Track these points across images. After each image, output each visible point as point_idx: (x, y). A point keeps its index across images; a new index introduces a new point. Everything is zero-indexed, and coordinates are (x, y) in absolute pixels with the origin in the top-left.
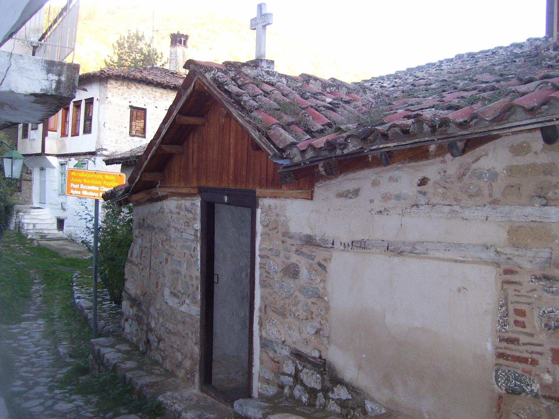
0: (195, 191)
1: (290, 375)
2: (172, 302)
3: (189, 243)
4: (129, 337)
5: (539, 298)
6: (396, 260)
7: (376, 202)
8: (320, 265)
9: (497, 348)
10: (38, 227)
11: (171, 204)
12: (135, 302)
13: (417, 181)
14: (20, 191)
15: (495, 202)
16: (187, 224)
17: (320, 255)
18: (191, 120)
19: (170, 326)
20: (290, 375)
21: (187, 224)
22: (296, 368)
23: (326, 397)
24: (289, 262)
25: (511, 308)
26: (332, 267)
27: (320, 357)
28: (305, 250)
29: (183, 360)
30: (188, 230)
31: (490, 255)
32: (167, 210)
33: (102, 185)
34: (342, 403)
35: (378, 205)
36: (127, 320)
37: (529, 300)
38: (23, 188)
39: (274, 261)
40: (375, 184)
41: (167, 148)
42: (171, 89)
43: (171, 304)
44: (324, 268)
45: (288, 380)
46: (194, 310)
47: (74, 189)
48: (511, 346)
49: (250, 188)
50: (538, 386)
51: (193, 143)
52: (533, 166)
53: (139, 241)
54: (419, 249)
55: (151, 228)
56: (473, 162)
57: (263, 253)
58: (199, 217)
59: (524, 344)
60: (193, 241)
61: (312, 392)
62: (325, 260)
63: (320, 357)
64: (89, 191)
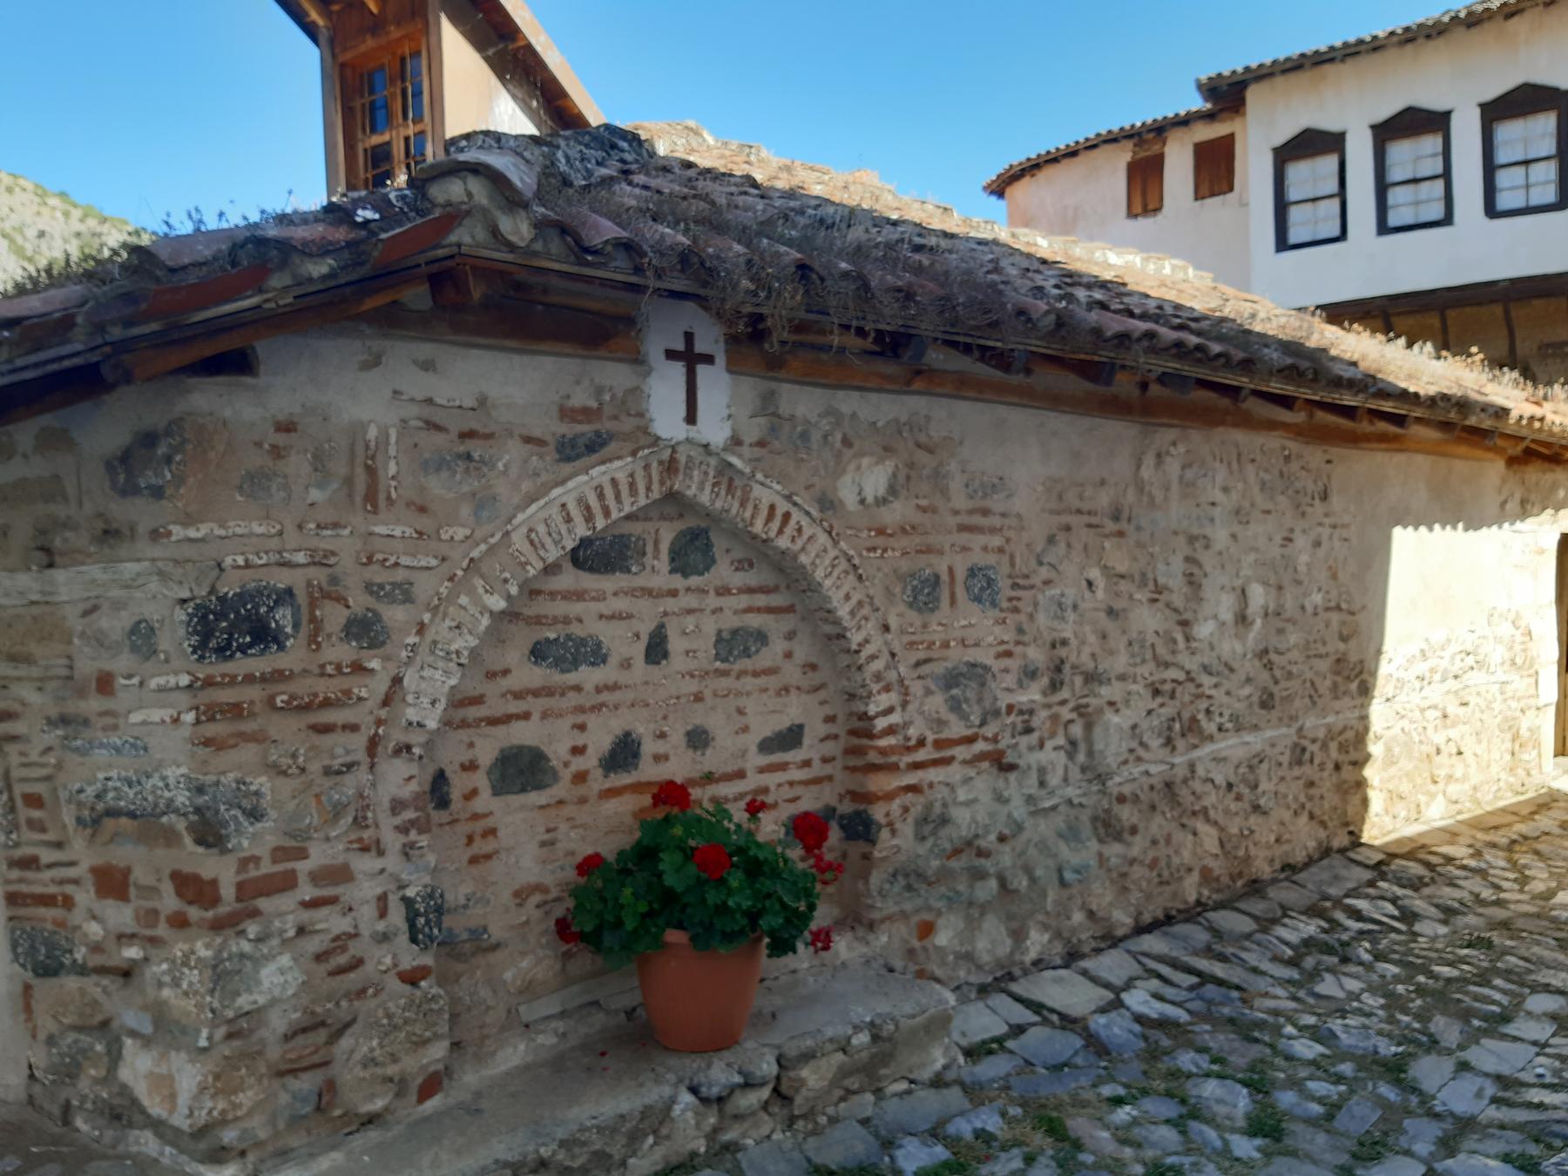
5: (59, 766)
25: (18, 790)
37: (44, 772)
42: (696, 279)
48: (30, 875)
50: (83, 949)
59: (50, 866)
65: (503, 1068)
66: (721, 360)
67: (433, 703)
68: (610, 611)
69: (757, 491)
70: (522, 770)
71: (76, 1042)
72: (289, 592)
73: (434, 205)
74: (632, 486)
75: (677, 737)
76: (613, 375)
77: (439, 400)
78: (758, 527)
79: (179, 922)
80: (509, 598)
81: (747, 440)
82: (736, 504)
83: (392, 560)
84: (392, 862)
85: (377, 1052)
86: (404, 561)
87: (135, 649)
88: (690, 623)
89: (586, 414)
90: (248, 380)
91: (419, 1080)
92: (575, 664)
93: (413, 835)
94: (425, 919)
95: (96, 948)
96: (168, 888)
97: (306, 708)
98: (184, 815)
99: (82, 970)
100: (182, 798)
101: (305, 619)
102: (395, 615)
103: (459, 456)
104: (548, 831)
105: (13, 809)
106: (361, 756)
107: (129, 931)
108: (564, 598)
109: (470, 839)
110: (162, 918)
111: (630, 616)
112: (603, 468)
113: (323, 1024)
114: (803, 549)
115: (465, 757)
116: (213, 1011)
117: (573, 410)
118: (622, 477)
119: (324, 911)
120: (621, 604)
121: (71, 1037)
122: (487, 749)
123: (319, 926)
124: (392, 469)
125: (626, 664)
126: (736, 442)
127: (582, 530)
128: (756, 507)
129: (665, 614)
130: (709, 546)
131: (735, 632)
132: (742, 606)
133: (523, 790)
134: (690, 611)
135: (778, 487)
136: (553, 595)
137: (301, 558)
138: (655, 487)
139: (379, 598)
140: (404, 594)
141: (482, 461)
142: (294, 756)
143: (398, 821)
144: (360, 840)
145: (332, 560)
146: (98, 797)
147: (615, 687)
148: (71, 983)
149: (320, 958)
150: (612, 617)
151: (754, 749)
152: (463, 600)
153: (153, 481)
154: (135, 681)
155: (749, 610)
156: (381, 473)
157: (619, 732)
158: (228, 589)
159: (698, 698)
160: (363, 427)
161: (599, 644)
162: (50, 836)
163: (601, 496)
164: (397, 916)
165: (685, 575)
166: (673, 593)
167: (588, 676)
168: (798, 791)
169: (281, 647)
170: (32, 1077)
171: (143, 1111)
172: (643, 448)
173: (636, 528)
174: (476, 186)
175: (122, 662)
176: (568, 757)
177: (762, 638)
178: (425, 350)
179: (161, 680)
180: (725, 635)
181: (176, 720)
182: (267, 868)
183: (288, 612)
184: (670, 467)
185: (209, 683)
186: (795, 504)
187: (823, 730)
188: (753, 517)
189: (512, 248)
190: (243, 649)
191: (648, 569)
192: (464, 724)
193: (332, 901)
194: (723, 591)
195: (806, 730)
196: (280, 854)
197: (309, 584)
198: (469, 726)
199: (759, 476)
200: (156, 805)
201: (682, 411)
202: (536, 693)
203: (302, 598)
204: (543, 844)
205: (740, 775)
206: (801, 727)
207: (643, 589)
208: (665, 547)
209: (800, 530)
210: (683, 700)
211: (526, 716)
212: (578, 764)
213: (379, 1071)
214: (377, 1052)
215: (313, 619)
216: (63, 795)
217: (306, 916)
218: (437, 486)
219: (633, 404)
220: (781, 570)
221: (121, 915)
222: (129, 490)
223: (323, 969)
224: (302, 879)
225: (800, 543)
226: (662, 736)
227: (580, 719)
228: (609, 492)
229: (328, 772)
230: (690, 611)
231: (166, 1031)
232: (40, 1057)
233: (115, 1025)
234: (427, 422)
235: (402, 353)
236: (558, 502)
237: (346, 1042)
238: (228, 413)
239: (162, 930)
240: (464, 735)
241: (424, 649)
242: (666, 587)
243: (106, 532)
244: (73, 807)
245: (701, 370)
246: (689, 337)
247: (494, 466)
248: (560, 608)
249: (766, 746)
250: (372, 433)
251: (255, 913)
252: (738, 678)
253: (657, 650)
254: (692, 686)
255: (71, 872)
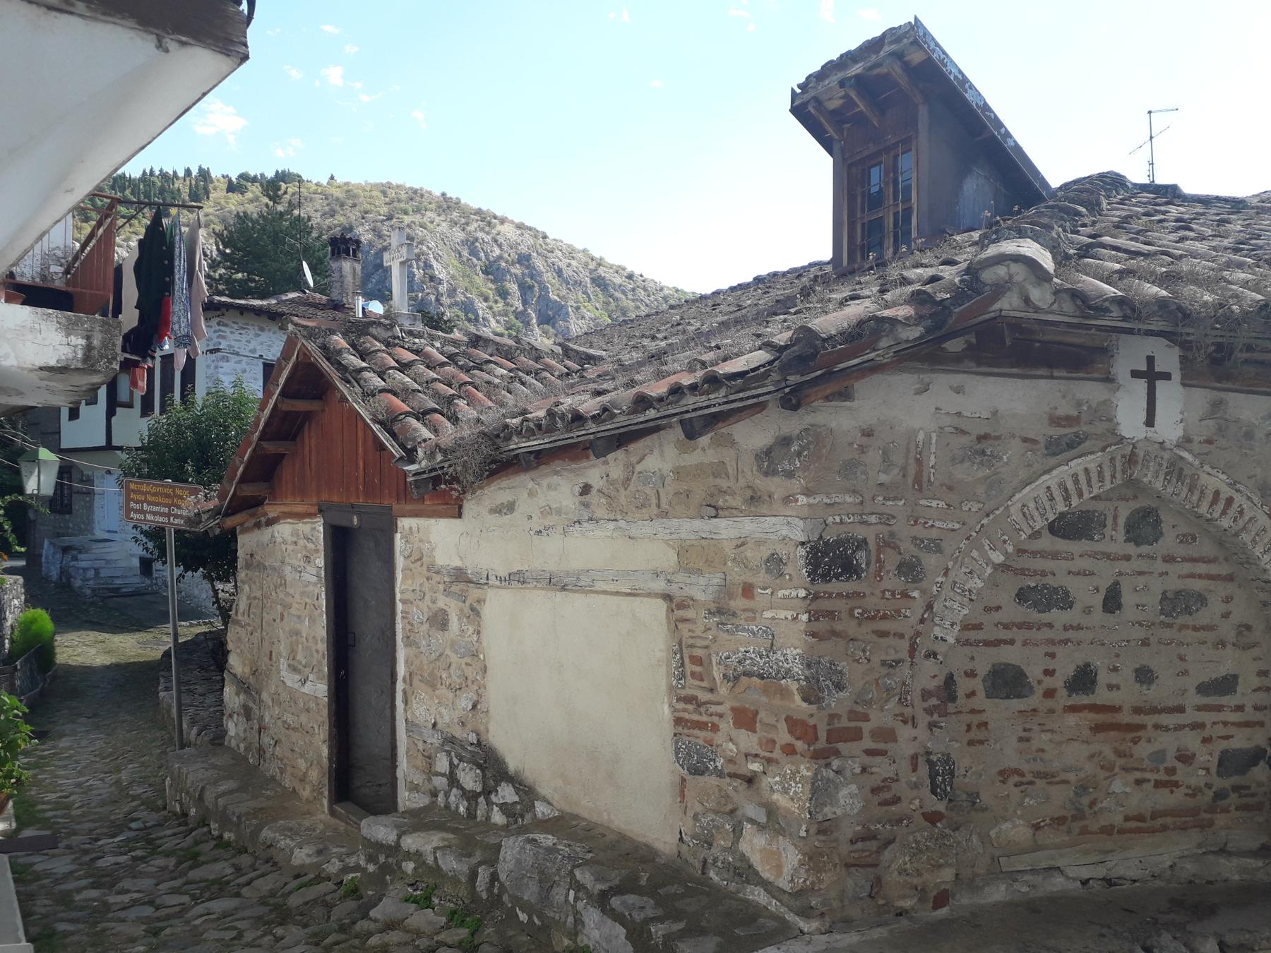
0: (314, 510)
1: (443, 775)
2: (291, 680)
3: (311, 588)
4: (233, 743)
5: (715, 640)
6: (560, 596)
7: (535, 518)
8: (472, 609)
9: (675, 710)
10: (103, 573)
11: (284, 530)
12: (243, 686)
13: (577, 490)
14: (70, 512)
15: (665, 515)
16: (308, 559)
17: (474, 593)
18: (301, 406)
19: (290, 719)
20: (443, 775)
21: (308, 559)
22: (451, 763)
23: (489, 803)
24: (435, 607)
26: (488, 611)
27: (479, 743)
28: (455, 588)
29: (307, 769)
30: (308, 568)
31: (659, 585)
32: (279, 540)
33: (173, 504)
34: (505, 808)
35: (536, 524)
36: (231, 716)
37: (705, 643)
38: (76, 507)
39: (417, 607)
40: (532, 494)
41: (271, 447)
43: (289, 684)
44: (478, 614)
45: (440, 782)
46: (319, 689)
47: (136, 511)
49: (386, 503)
51: (311, 439)
52: (700, 466)
53: (246, 588)
54: (585, 581)
55: (261, 567)
56: (638, 462)
57: (406, 597)
58: (321, 547)
60: (315, 584)
61: (471, 797)
62: (478, 601)
63: (479, 743)
64: (155, 514)
65: (983, 902)
66: (1176, 376)
67: (952, 625)
68: (1080, 570)
69: (1204, 479)
70: (1008, 682)
71: (713, 820)
72: (865, 541)
73: (986, 285)
74: (1100, 474)
75: (1127, 673)
76: (1090, 391)
77: (965, 413)
78: (1203, 509)
79: (789, 750)
80: (1006, 554)
81: (1197, 439)
82: (1185, 490)
83: (930, 523)
84: (921, 732)
85: (908, 866)
86: (938, 524)
87: (768, 571)
88: (1141, 581)
89: (1070, 420)
90: (847, 403)
91: (934, 893)
92: (1048, 608)
93: (936, 716)
94: (940, 775)
95: (731, 761)
96: (783, 726)
97: (873, 618)
98: (798, 680)
99: (720, 774)
100: (797, 669)
101: (873, 559)
102: (931, 561)
103: (976, 452)
104: (1025, 730)
105: (683, 665)
106: (904, 655)
107: (754, 752)
108: (1042, 557)
109: (969, 728)
110: (778, 746)
111: (1092, 574)
112: (1080, 460)
113: (874, 837)
114: (1244, 528)
115: (969, 667)
116: (810, 813)
117: (1059, 418)
118: (1092, 467)
119: (878, 759)
120: (1086, 564)
121: (711, 816)
122: (984, 662)
123: (874, 770)
124: (932, 460)
125: (1088, 610)
126: (1186, 441)
127: (1061, 507)
128: (1202, 492)
129: (1120, 574)
130: (1158, 522)
131: (1178, 593)
132: (1185, 572)
133: (1008, 697)
134: (1141, 573)
135: (1224, 477)
136: (1034, 554)
137: (873, 519)
138: (1118, 475)
139: (920, 549)
140: (935, 546)
141: (992, 456)
142: (864, 651)
143: (926, 705)
144: (902, 715)
145: (892, 522)
146: (739, 662)
147: (1079, 628)
148: (711, 781)
149: (875, 791)
150: (1079, 574)
151: (1192, 691)
152: (975, 554)
153: (788, 467)
154: (768, 591)
155: (1192, 576)
156: (925, 463)
157: (1081, 664)
158: (830, 536)
159: (1145, 643)
160: (915, 433)
161: (1067, 594)
162: (704, 684)
163: (1076, 482)
164: (924, 770)
165: (1138, 544)
166: (1127, 558)
167: (1057, 616)
168: (1231, 730)
169: (859, 577)
170: (681, 839)
171: (757, 873)
172: (1110, 445)
173: (1100, 506)
174: (1015, 267)
175: (761, 578)
176: (1041, 677)
177: (1202, 599)
178: (957, 379)
179: (787, 592)
180: (1169, 595)
181: (795, 619)
182: (845, 723)
183: (864, 554)
184: (1131, 460)
185: (816, 597)
186: (1238, 491)
187: (1256, 682)
188: (1199, 500)
189: (1037, 310)
190: (837, 576)
191: (1108, 537)
192: (967, 643)
193: (882, 753)
194: (1169, 559)
195: (1240, 680)
196: (854, 716)
197: (877, 536)
198: (971, 645)
199: (1207, 468)
200: (779, 672)
201: (1143, 416)
202: (1020, 626)
203: (872, 546)
204: (1021, 739)
205: (1180, 709)
206: (1235, 677)
207: (1103, 553)
208: (1122, 521)
209: (1241, 513)
210: (1133, 643)
211: (1012, 642)
212: (1049, 682)
213: (909, 879)
214: (908, 866)
215: (878, 560)
216: (714, 659)
217: (868, 760)
218: (962, 473)
219: (1104, 414)
220: (1221, 544)
221: (748, 740)
222: (770, 472)
223: (876, 799)
224: (866, 734)
225: (1241, 523)
226: (1115, 669)
227: (1051, 649)
228: (1082, 478)
229: (884, 663)
230: (1141, 573)
231: (774, 822)
232: (688, 826)
233: (739, 813)
234: (956, 429)
235: (942, 382)
236: (1044, 486)
237: (887, 854)
238: (833, 425)
239: (777, 754)
240: (967, 650)
241: (947, 586)
242: (1121, 553)
243: (752, 498)
244: (722, 668)
245: (1160, 385)
246: (1151, 360)
247: (1001, 458)
248: (1039, 564)
249: (1203, 689)
250: (921, 436)
251: (837, 753)
252: (1180, 630)
253: (1112, 601)
254: (1140, 633)
255: (719, 709)
